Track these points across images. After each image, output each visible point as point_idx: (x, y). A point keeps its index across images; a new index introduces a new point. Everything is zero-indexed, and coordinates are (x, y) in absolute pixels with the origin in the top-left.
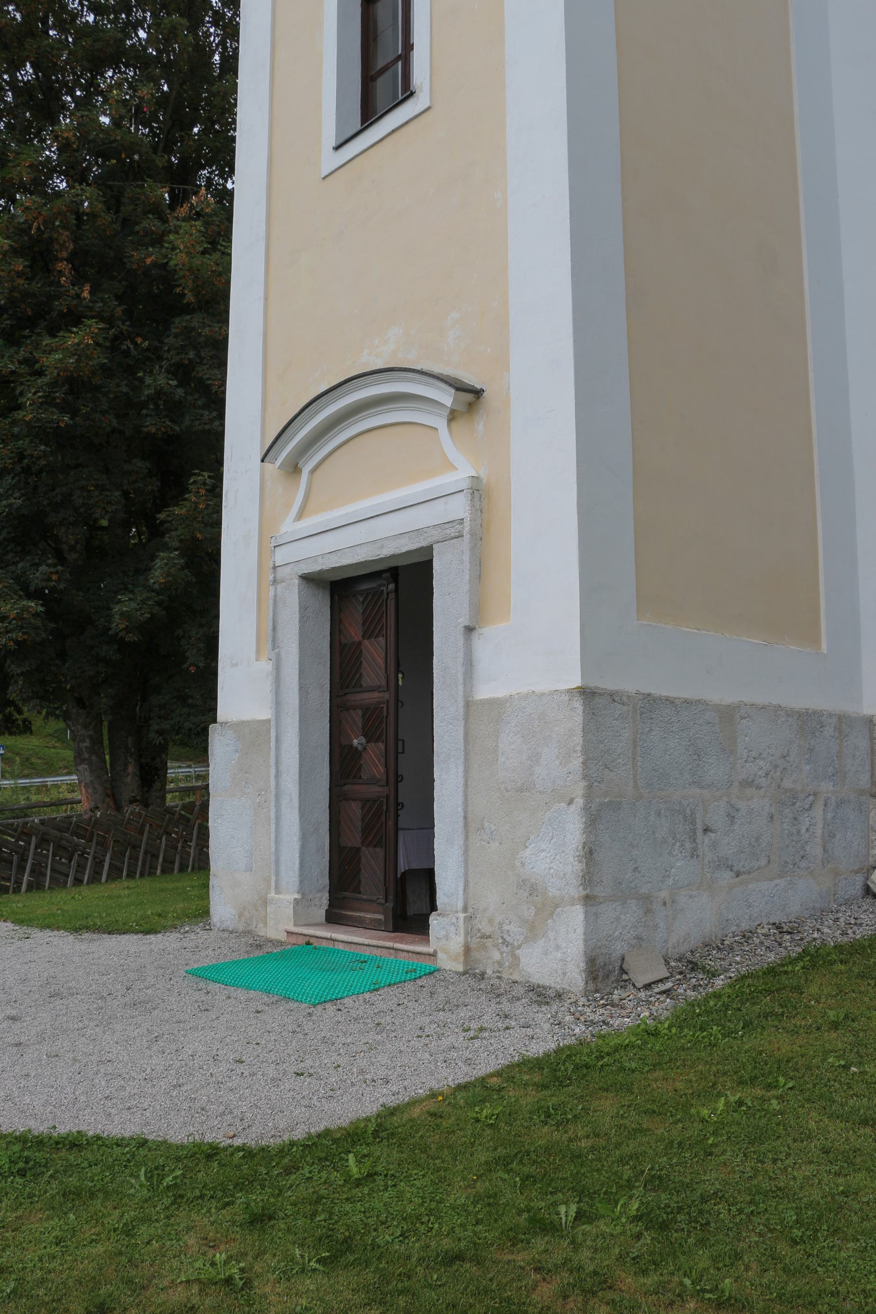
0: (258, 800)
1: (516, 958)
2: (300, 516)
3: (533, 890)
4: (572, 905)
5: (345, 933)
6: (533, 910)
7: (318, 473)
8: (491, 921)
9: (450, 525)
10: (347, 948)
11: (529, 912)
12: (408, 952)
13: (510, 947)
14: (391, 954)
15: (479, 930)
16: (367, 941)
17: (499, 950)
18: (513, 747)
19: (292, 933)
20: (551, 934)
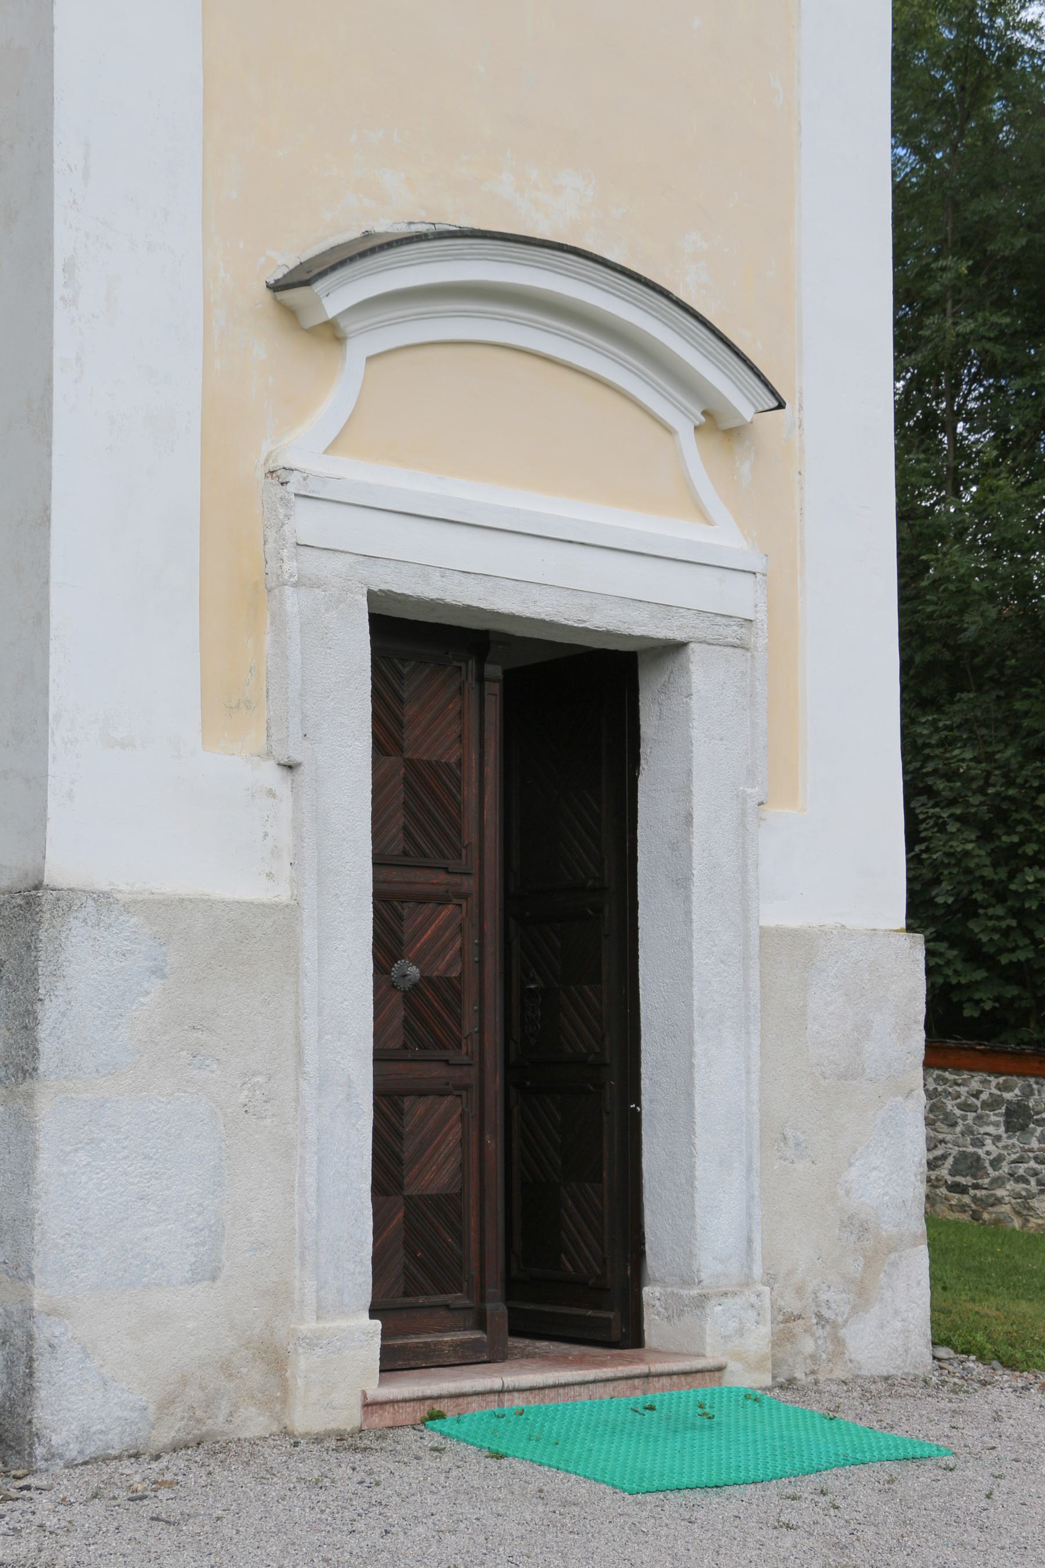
0: (242, 1098)
1: (839, 1342)
3: (864, 1228)
4: (915, 1245)
5: (533, 1371)
6: (861, 1261)
8: (799, 1291)
9: (724, 621)
10: (535, 1399)
11: (854, 1267)
12: (670, 1374)
13: (828, 1328)
14: (635, 1388)
16: (591, 1374)
17: (813, 1335)
18: (831, 1009)
19: (381, 1404)
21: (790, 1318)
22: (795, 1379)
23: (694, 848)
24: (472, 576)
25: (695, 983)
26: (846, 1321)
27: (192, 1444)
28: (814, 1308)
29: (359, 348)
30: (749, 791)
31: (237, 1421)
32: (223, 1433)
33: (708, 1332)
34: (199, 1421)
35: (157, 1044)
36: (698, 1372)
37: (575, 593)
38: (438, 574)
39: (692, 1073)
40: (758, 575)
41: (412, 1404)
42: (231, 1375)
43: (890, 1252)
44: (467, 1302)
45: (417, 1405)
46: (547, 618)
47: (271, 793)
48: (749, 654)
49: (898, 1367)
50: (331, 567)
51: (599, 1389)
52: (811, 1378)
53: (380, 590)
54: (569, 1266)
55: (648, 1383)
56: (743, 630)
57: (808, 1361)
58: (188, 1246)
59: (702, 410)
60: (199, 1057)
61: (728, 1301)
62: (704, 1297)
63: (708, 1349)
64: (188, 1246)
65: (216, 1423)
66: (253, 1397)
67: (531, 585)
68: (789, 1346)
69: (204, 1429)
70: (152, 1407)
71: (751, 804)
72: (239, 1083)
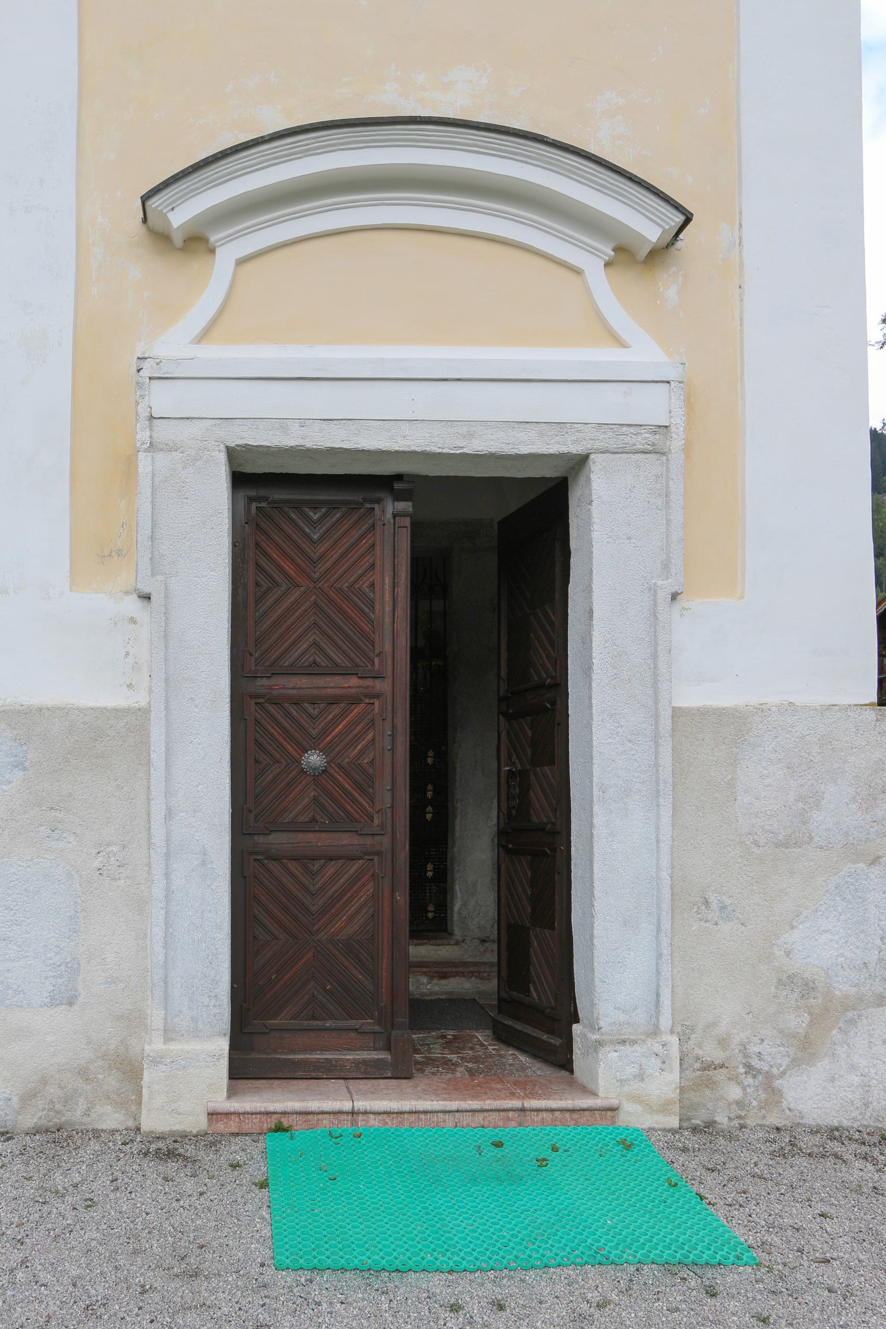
0: (97, 863)
2: (203, 336)
3: (808, 988)
7: (250, 267)
9: (632, 430)
11: (797, 1022)
13: (760, 1078)
14: (509, 1119)
15: (697, 1058)
19: (228, 1114)
20: (841, 1051)
21: (710, 1066)
22: (715, 1122)
23: (594, 639)
24: (335, 422)
25: (594, 761)
26: (783, 1073)
27: (53, 1130)
28: (740, 1058)
29: (228, 252)
30: (660, 583)
31: (94, 1116)
32: (81, 1124)
33: (600, 1075)
34: (58, 1112)
35: (17, 821)
36: (584, 1110)
37: (449, 423)
38: (297, 425)
39: (592, 843)
40: (672, 383)
41: (258, 1116)
42: (87, 1079)
43: (847, 1010)
44: (377, 1028)
45: (264, 1118)
46: (419, 449)
47: (133, 621)
48: (665, 458)
49: (855, 1119)
50: (187, 432)
51: (467, 1118)
52: (736, 1123)
53: (238, 446)
54: (535, 995)
55: (525, 1116)
56: (657, 437)
57: (734, 1106)
58: (46, 978)
59: (612, 246)
60: (57, 831)
61: (627, 1049)
62: (600, 1043)
63: (601, 1089)
64: (46, 978)
65: (76, 1114)
66: (109, 1098)
67: (400, 422)
68: (708, 1092)
69: (63, 1119)
70: (15, 1099)
71: (663, 596)
72: (95, 851)
